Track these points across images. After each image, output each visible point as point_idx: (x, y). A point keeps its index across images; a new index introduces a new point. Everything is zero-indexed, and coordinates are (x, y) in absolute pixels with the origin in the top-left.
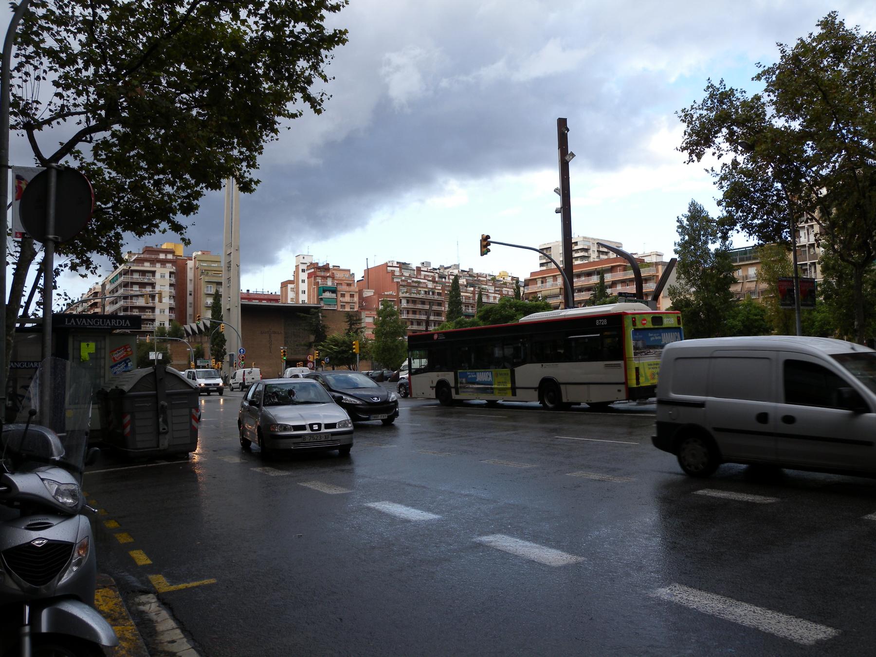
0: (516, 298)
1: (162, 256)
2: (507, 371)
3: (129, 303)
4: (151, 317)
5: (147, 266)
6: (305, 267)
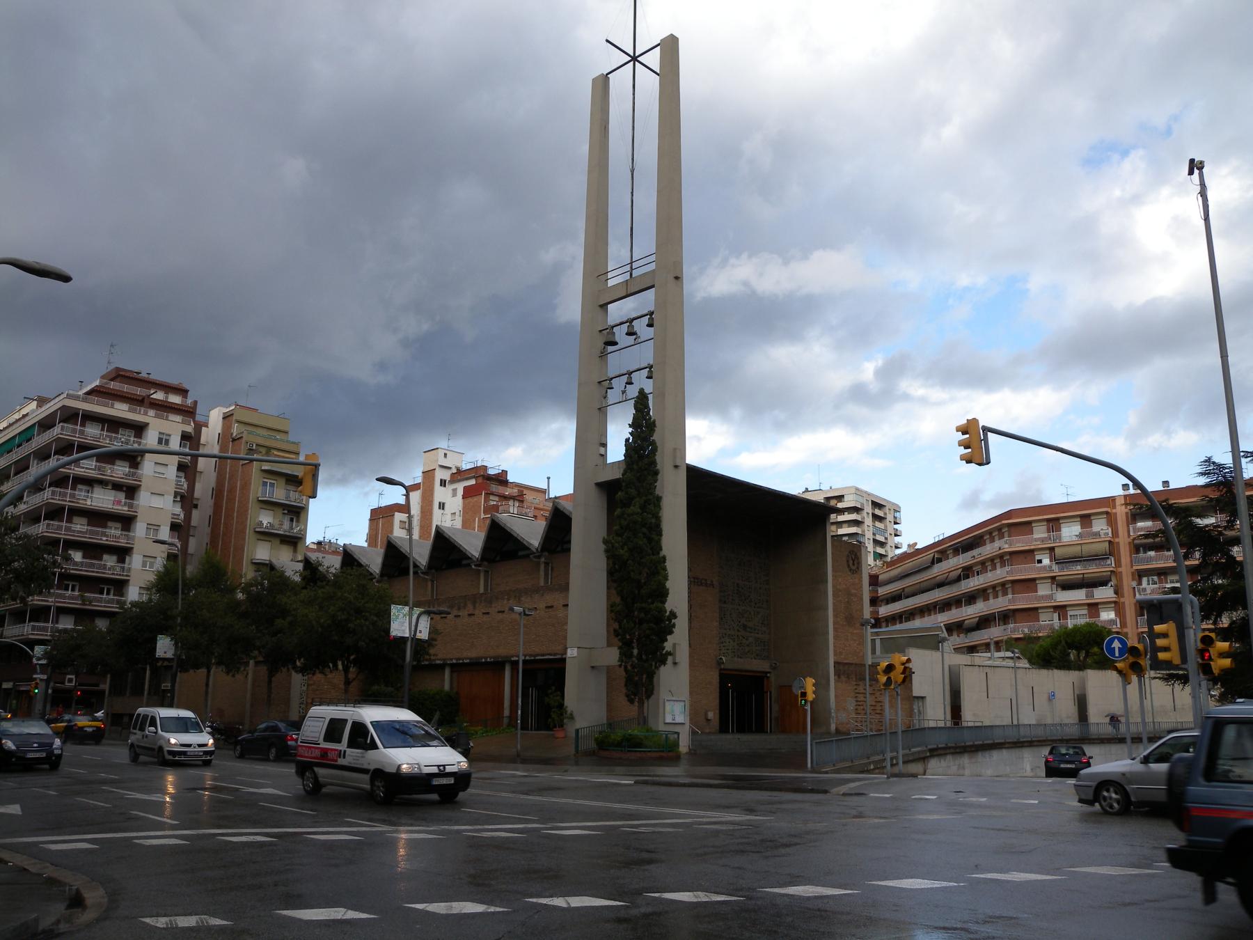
0: (184, 585)
1: (159, 396)
2: (969, 716)
3: (63, 497)
4: (123, 542)
5: (120, 410)
6: (446, 475)
